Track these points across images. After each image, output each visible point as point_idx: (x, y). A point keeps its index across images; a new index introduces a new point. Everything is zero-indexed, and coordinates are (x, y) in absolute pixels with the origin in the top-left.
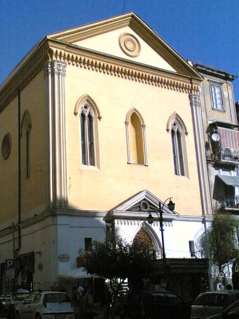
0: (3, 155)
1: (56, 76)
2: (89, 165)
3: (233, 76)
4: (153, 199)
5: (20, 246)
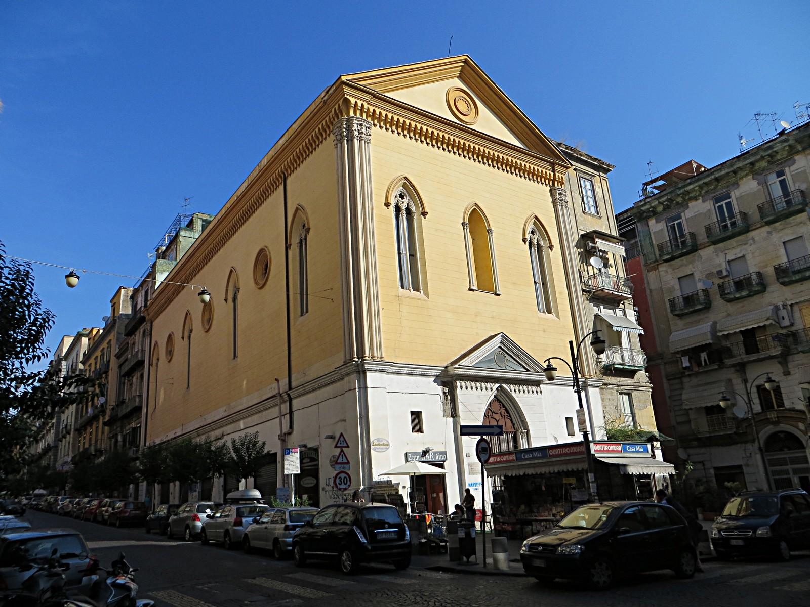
0: (256, 283)
1: (356, 142)
2: (412, 290)
3: (609, 166)
4: (515, 350)
5: (291, 427)
